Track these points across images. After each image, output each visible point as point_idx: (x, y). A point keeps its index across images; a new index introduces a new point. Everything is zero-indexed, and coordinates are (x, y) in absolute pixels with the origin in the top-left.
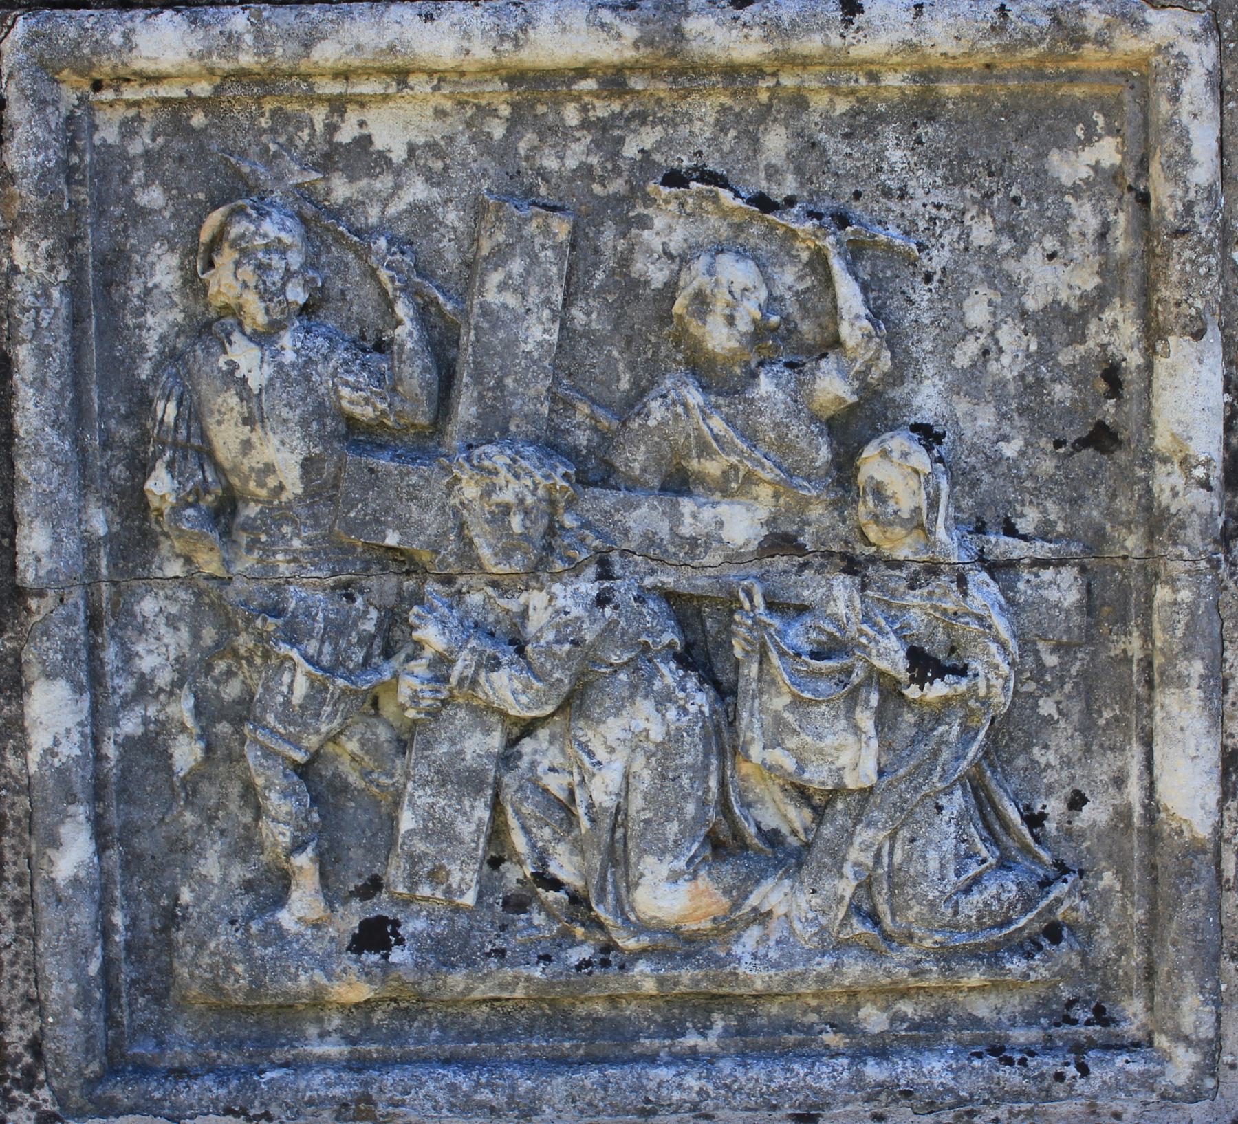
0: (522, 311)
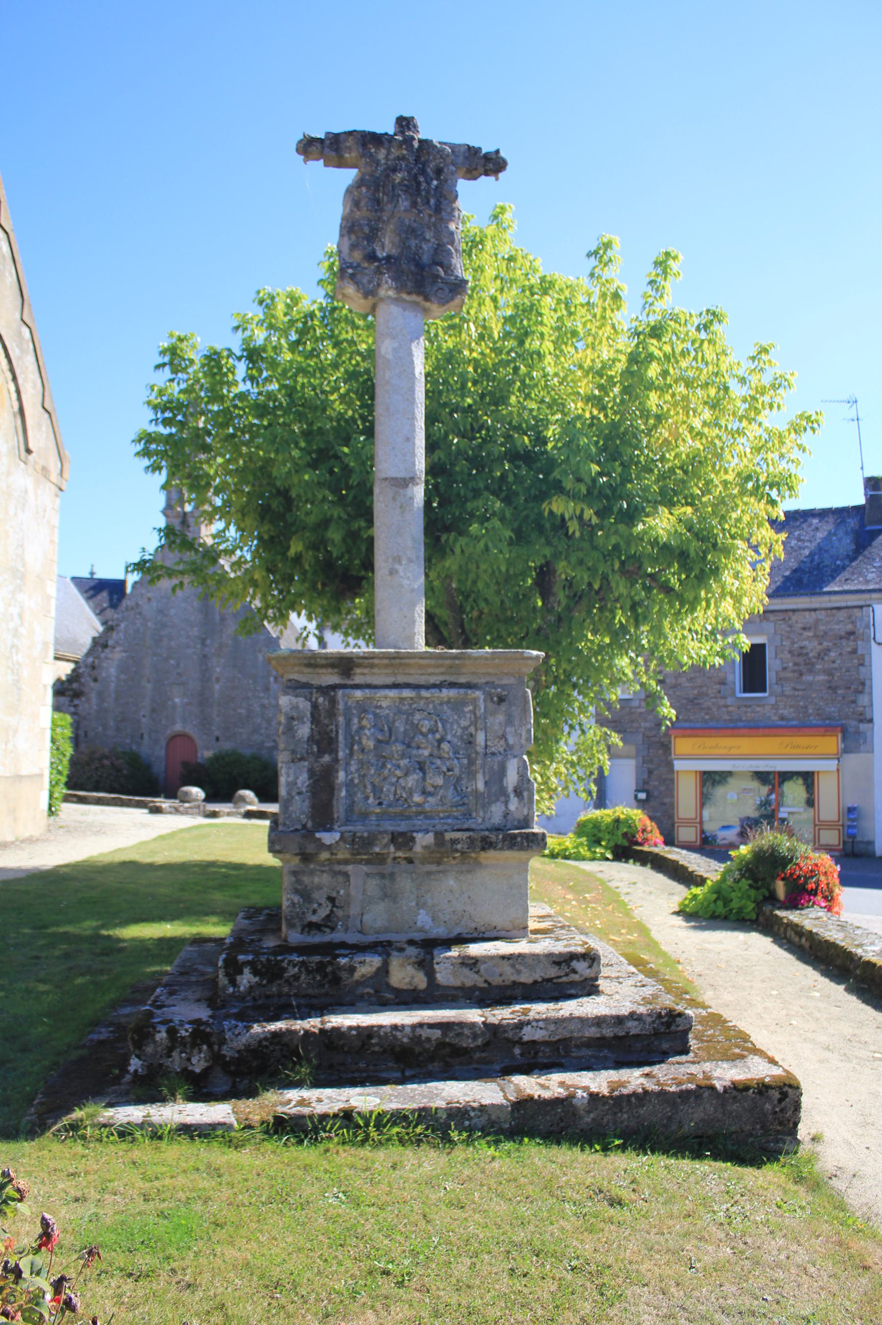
0: (400, 726)
